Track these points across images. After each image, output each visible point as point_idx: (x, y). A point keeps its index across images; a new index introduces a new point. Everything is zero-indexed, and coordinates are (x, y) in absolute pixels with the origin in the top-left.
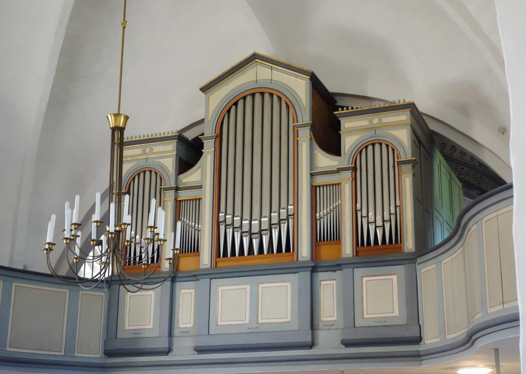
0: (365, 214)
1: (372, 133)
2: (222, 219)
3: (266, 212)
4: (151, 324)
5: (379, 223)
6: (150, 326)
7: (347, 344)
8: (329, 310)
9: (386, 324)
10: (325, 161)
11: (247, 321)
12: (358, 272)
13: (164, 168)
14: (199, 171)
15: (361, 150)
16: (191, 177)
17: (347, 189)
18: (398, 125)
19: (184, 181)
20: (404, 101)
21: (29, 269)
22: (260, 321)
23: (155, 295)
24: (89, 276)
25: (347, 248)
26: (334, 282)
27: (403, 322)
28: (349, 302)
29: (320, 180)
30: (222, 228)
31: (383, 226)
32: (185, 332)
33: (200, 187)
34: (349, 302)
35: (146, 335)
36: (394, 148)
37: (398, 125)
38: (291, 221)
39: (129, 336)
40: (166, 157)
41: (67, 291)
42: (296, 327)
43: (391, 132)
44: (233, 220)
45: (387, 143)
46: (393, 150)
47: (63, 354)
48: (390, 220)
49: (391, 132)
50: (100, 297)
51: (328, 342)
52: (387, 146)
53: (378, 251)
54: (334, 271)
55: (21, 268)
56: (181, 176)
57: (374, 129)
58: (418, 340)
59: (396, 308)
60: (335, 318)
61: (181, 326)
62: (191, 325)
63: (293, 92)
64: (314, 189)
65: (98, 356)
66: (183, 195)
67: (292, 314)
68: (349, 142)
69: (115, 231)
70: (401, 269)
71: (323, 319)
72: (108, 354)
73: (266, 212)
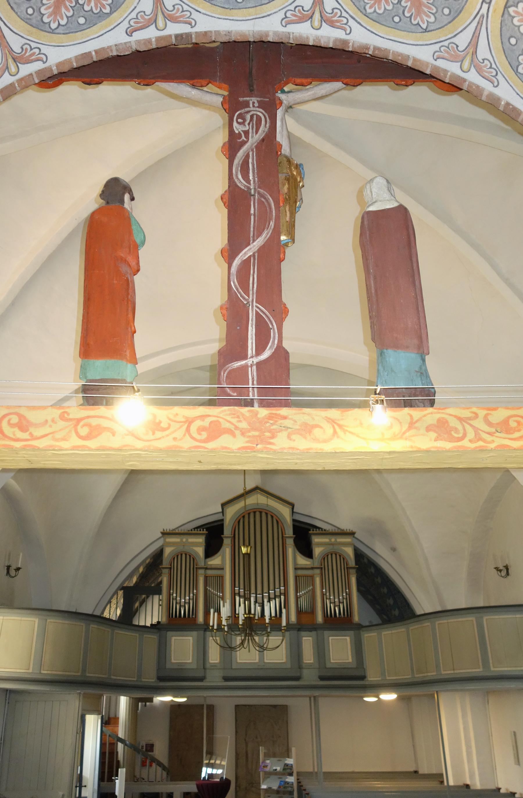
0: (328, 597)
1: (331, 547)
2: (237, 592)
3: (266, 590)
4: (191, 659)
5: (337, 603)
6: (190, 661)
7: (322, 678)
8: (309, 656)
9: (345, 667)
10: (302, 561)
11: (257, 661)
12: (326, 633)
13: (196, 553)
14: (220, 558)
15: (325, 557)
16: (215, 561)
17: (318, 580)
18: (197, 545)
19: (210, 563)
20: (349, 530)
21: (77, 611)
22: (266, 661)
23: (193, 640)
24: (142, 623)
25: (320, 618)
26: (310, 638)
27: (354, 666)
28: (321, 651)
29: (300, 572)
30: (237, 598)
31: (339, 606)
32: (214, 666)
33: (223, 569)
34: (321, 651)
35: (188, 667)
36: (278, 520)
37: (197, 545)
38: (282, 597)
39: (175, 667)
40: (197, 545)
41: (138, 635)
42: (289, 666)
43: (343, 548)
44: (239, 591)
45: (267, 512)
46: (344, 559)
47: (135, 679)
48: (343, 602)
49: (343, 548)
50: (153, 638)
51: (310, 677)
52: (340, 556)
53: (339, 622)
54: (311, 631)
55: (74, 611)
56: (208, 560)
57: (332, 544)
58: (363, 678)
59: (350, 657)
60: (312, 661)
61: (211, 661)
62: (218, 661)
63: (282, 515)
64: (296, 577)
65: (153, 681)
66: (210, 572)
67: (286, 658)
68: (317, 551)
69: (245, 618)
70: (352, 633)
71: (305, 662)
72: (160, 679)
73: (266, 590)
